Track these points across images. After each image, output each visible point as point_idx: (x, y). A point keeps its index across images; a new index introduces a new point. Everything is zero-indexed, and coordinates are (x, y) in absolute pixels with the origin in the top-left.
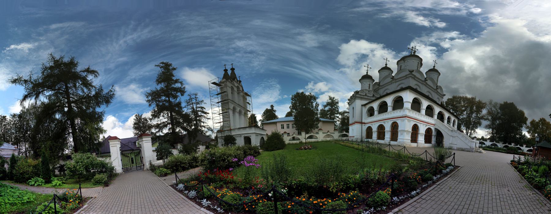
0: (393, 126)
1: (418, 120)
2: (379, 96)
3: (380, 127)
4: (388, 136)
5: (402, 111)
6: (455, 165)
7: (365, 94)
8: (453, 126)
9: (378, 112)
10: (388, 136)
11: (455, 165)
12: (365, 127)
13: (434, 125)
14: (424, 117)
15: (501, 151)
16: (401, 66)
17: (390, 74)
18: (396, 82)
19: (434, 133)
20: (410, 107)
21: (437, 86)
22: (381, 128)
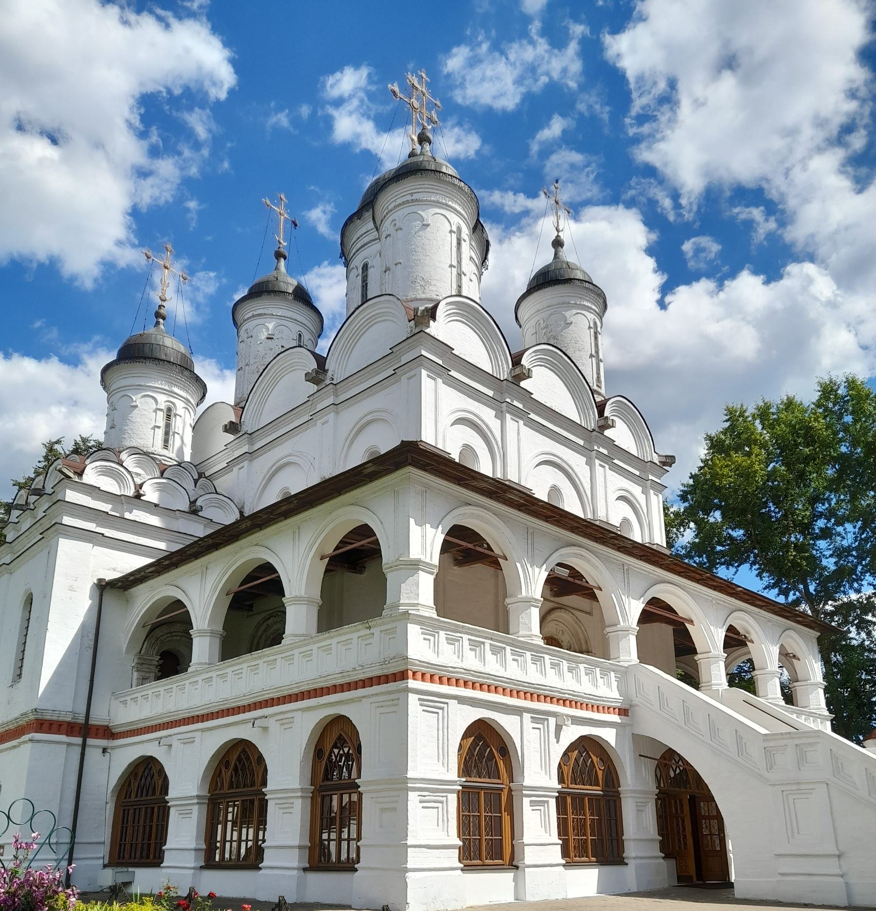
2: (229, 517)
5: (376, 631)
7: (131, 492)
9: (217, 642)
16: (365, 267)
17: (307, 337)
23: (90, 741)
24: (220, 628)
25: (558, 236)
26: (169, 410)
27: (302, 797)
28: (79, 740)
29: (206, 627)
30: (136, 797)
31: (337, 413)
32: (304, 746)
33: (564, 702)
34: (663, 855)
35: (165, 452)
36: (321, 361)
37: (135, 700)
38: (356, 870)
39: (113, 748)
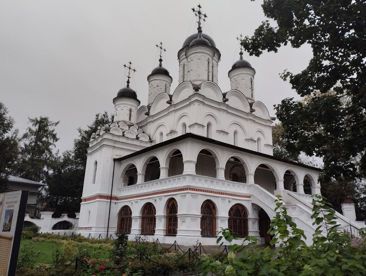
0: (170, 205)
1: (212, 192)
3: (148, 207)
4: (161, 225)
8: (6, 264)
9: (144, 176)
10: (161, 225)
12: (117, 208)
13: (249, 197)
16: (184, 65)
18: (175, 111)
19: (252, 215)
22: (149, 209)
23: (112, 201)
24: (144, 173)
25: (241, 51)
27: (164, 218)
28: (109, 201)
29: (141, 173)
30: (124, 216)
31: (175, 112)
32: (165, 205)
33: (231, 195)
34: (260, 236)
36: (171, 97)
37: (123, 190)
38: (176, 236)
39: (117, 203)
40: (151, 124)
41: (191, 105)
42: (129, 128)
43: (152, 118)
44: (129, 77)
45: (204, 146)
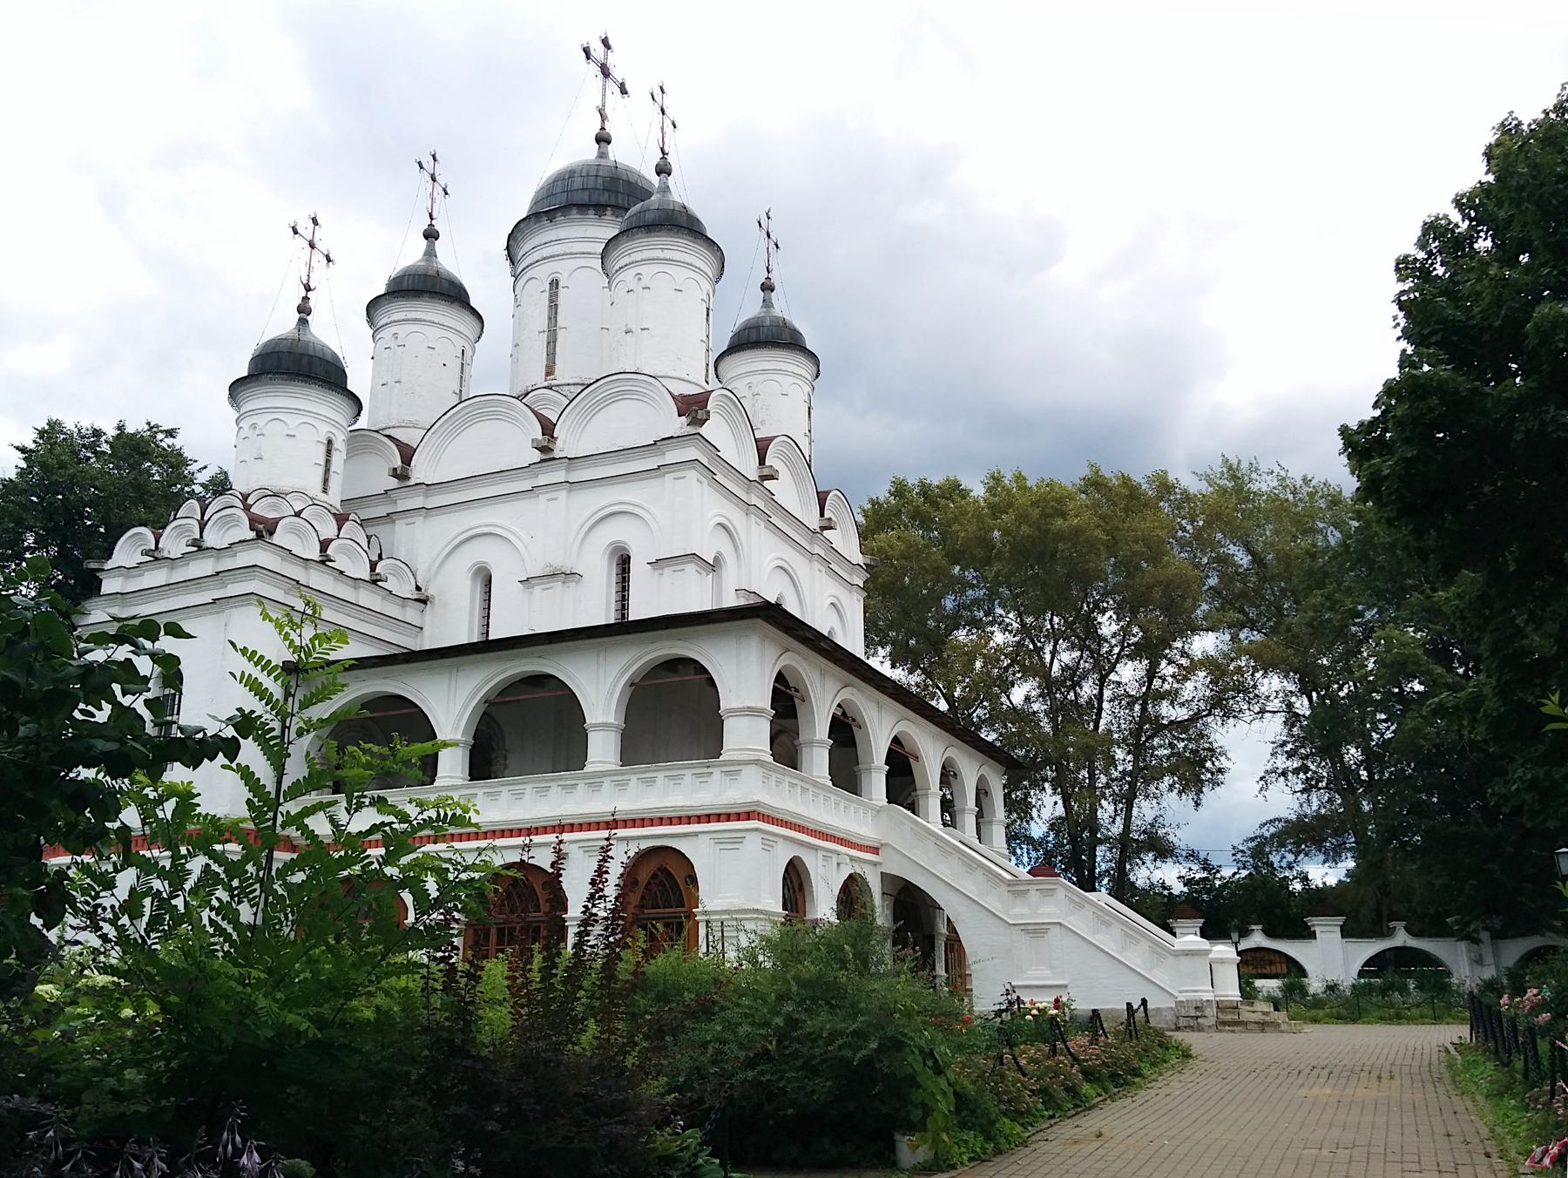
6: (1152, 1024)
11: (1152, 1024)
13: (875, 851)
14: (826, 799)
15: (373, 661)
20: (768, 749)
21: (762, 447)
26: (330, 442)
35: (323, 497)
40: (419, 520)
41: (663, 475)
42: (339, 530)
43: (426, 496)
44: (308, 289)
45: (651, 647)
